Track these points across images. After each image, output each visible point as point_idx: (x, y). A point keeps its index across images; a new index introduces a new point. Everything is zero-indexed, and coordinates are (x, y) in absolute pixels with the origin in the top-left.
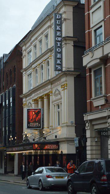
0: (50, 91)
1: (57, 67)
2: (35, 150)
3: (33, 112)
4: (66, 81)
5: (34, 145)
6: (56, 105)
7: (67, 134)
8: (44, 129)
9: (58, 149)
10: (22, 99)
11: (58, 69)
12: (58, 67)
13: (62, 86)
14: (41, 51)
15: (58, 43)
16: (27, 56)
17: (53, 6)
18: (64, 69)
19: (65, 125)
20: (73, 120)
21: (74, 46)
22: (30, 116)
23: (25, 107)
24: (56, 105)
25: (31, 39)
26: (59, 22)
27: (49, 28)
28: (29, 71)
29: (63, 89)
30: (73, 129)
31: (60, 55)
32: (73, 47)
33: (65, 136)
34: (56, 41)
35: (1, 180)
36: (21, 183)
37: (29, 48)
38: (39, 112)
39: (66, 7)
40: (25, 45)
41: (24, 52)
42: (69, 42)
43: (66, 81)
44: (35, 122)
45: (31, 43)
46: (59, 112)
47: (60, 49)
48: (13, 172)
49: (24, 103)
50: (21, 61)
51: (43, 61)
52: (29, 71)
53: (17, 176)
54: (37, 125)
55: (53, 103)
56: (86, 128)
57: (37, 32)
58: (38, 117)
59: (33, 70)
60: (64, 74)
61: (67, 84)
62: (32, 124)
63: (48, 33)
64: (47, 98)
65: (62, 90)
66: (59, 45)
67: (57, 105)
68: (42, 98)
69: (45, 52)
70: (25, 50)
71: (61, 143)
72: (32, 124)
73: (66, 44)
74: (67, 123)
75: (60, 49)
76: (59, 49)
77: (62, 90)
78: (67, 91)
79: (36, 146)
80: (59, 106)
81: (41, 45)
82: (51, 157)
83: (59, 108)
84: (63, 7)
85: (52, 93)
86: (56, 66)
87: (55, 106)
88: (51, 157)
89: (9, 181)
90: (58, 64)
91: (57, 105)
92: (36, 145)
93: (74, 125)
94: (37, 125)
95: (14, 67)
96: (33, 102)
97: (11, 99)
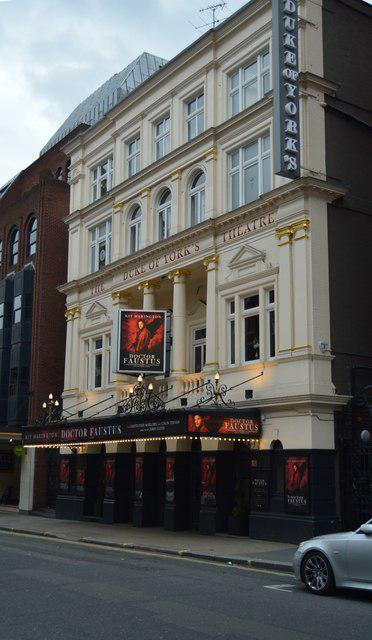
0: (212, 257)
1: (288, 163)
2: (193, 434)
3: (140, 323)
4: (306, 212)
5: (190, 419)
6: (91, 340)
8: (173, 375)
9: (258, 435)
10: (63, 297)
11: (289, 167)
13: (278, 230)
14: (130, 169)
16: (87, 178)
17: (120, 89)
19: (305, 352)
20: (327, 340)
21: (327, 109)
22: (129, 332)
23: (73, 320)
25: (113, 124)
26: (291, 21)
27: (207, 72)
29: (286, 239)
30: (326, 368)
31: (295, 125)
32: (322, 112)
33: (306, 391)
36: (126, 547)
37: (107, 150)
38: (159, 323)
40: (84, 147)
41: (79, 168)
42: (314, 93)
43: (306, 212)
44: (145, 351)
45: (116, 136)
48: (15, 501)
49: (69, 308)
50: (64, 189)
51: (143, 191)
52: (102, 215)
53: (30, 513)
54: (149, 361)
57: (198, 59)
58: (156, 336)
59: (119, 209)
60: (302, 188)
62: (133, 359)
63: (139, 133)
64: (183, 283)
65: (115, 305)
66: (291, 93)
67: (265, 289)
69: (154, 164)
70: (83, 162)
72: (133, 359)
74: (309, 346)
77: (115, 305)
78: (310, 244)
79: (197, 420)
80: (272, 294)
81: (158, 134)
82: (139, 462)
85: (79, 312)
86: (282, 159)
88: (139, 462)
90: (291, 153)
92: (196, 417)
93: (329, 354)
94: (149, 361)
95: (30, 216)
96: (117, 300)
97: (18, 302)
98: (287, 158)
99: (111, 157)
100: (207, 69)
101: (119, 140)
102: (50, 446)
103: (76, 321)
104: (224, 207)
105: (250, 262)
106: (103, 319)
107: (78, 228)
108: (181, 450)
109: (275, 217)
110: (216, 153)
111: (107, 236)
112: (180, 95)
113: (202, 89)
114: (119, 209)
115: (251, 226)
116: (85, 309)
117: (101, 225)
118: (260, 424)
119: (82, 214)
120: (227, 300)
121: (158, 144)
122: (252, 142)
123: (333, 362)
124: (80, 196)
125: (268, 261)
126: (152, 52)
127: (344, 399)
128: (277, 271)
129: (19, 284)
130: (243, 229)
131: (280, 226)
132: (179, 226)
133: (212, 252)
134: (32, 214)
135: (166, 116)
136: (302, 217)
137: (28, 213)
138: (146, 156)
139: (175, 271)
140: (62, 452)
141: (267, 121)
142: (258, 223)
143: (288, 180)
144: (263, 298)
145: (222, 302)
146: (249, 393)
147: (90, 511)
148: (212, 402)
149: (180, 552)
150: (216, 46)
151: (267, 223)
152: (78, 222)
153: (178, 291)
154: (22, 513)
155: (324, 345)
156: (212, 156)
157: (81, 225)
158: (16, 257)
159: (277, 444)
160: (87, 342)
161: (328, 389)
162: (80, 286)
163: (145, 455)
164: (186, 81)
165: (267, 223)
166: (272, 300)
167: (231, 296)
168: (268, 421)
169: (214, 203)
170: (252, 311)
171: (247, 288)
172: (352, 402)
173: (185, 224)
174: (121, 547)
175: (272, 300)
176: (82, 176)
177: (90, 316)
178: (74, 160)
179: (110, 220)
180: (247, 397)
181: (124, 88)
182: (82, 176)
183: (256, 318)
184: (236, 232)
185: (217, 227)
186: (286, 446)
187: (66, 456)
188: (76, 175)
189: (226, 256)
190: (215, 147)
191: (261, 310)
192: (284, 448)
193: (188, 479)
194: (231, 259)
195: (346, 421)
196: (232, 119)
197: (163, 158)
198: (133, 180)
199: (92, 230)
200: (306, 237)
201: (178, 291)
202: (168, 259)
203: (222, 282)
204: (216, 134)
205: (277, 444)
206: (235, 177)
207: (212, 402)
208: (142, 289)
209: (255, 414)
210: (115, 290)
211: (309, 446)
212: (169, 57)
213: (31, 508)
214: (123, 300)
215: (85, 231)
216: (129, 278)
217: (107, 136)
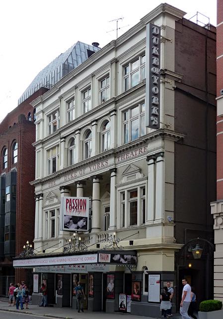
7: (162, 239)
10: (33, 187)
11: (154, 123)
12: (155, 120)
15: (155, 77)
18: (161, 126)
24: (48, 212)
26: (157, 40)
28: (50, 145)
34: (152, 74)
35: (2, 310)
39: (166, 18)
46: (144, 201)
47: (157, 89)
52: (50, 145)
55: (44, 209)
56: (215, 227)
61: (163, 153)
63: (145, 51)
66: (155, 81)
67: (141, 188)
68: (86, 185)
70: (43, 112)
71: (141, 253)
73: (164, 83)
75: (157, 89)
76: (156, 89)
83: (144, 194)
84: (160, 17)
87: (47, 212)
89: (31, 314)
91: (141, 188)
95: (13, 142)
100: (111, 62)
119: (42, 142)
127: (179, 246)
134: (15, 140)
145: (119, 193)
156: (113, 113)
167: (136, 187)
170: (133, 199)
180: (130, 244)
184: (125, 157)
188: (39, 119)
202: (134, 153)
217: (56, 98)
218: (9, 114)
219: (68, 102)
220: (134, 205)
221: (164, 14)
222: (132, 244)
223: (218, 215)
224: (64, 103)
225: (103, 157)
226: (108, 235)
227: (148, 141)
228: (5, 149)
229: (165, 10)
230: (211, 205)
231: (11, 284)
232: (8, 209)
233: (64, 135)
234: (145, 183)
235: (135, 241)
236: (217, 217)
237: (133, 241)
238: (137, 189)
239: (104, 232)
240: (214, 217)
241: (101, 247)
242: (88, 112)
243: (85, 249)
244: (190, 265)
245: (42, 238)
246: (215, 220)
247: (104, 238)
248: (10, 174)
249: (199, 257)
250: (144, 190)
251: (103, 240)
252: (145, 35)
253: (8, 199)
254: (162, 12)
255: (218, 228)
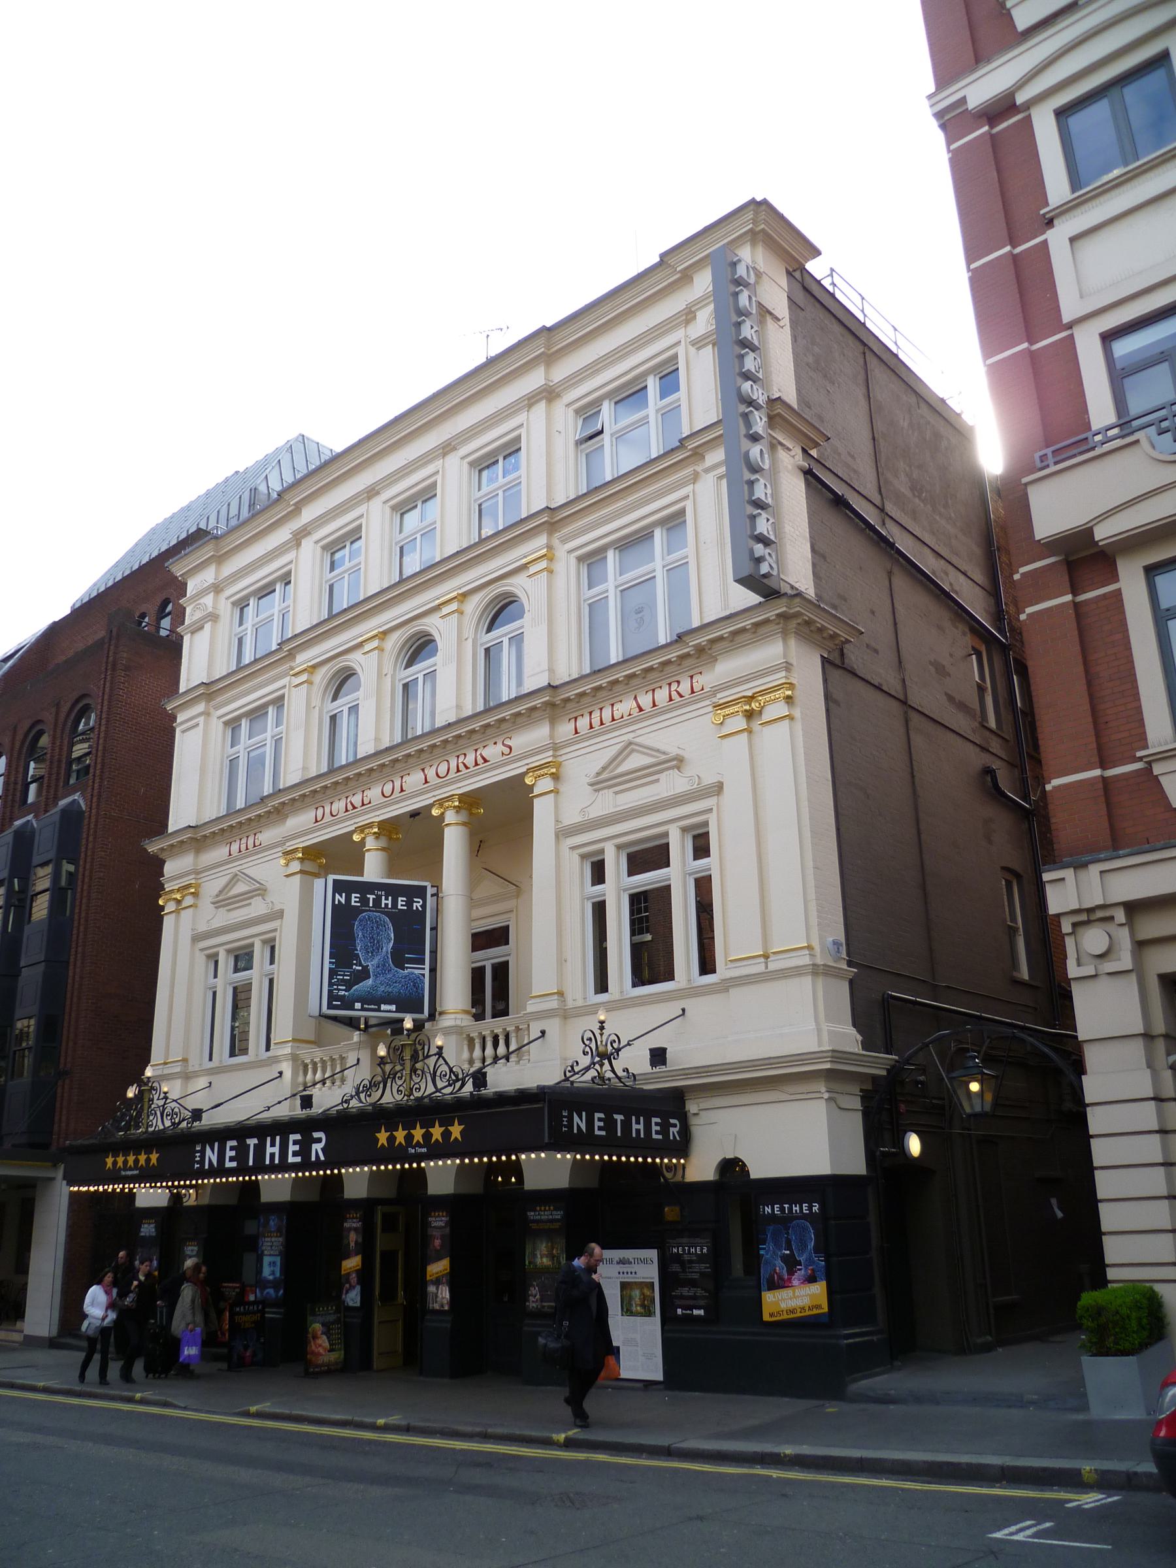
0: (189, 886)
4: (788, 667)
9: (683, 1147)
17: (255, 490)
19: (804, 960)
25: (297, 509)
27: (530, 406)
29: (739, 723)
33: (810, 1045)
41: (208, 600)
50: (173, 649)
64: (464, 824)
67: (264, 942)
70: (217, 588)
74: (809, 948)
87: (598, 874)
91: (264, 942)
95: (77, 701)
98: (759, 549)
99: (286, 580)
100: (530, 401)
101: (308, 544)
102: (118, 1188)
103: (186, 915)
104: (570, 665)
105: (246, 897)
106: (258, 907)
107: (201, 719)
108: (462, 1191)
109: (707, 679)
110: (551, 560)
111: (269, 734)
112: (464, 451)
113: (518, 439)
114: (304, 677)
115: (645, 700)
116: (212, 886)
117: (257, 714)
118: (684, 1118)
119: (210, 691)
120: (209, 957)
121: (331, 587)
122: (642, 537)
123: (851, 982)
124: (200, 660)
125: (689, 770)
126: (313, 434)
127: (879, 1064)
128: (719, 788)
129: (45, 846)
130: (625, 706)
131: (722, 697)
132: (305, 769)
133: (547, 757)
134: (39, 722)
135: (427, 494)
136: (779, 677)
137: (75, 695)
138: (373, 568)
139: (450, 798)
140: (140, 1203)
141: (767, 461)
142: (662, 695)
143: (754, 599)
144: (260, 954)
145: (201, 959)
146: (658, 1056)
147: (258, 1346)
148: (592, 1073)
149: (138, 1395)
150: (549, 359)
151: (357, 803)
152: (200, 707)
153: (454, 842)
154: (32, 1342)
155: (835, 943)
156: (543, 564)
157: (206, 714)
158: (33, 788)
159: (731, 1167)
160: (214, 959)
161: (850, 1039)
162: (200, 838)
163: (366, 1206)
164: (472, 428)
165: (357, 803)
166: (272, 962)
167: (215, 950)
168: (705, 1117)
169: (546, 651)
170: (648, 879)
171: (639, 828)
172: (894, 1072)
173: (390, 736)
174: (373, 1427)
175: (272, 962)
176: (213, 617)
177: (223, 901)
178: (192, 587)
179: (279, 702)
180: (654, 1063)
181: (262, 488)
182: (213, 617)
183: (248, 987)
184: (607, 714)
185: (555, 702)
186: (763, 1166)
187: (150, 1213)
188: (198, 615)
189: (583, 764)
190: (549, 557)
191: (255, 976)
192: (753, 1176)
193: (463, 1249)
194: (598, 768)
195: (883, 1108)
196: (505, 530)
197: (488, 538)
198: (335, 621)
199: (233, 725)
200: (790, 717)
201: (454, 842)
202: (431, 773)
203: (571, 817)
204: (552, 520)
205: (731, 1167)
206: (233, 762)
207: (592, 1073)
208: (363, 842)
209: (672, 1104)
210: (290, 846)
211: (822, 1167)
212: (339, 448)
213: (54, 1333)
214: (309, 866)
215: (216, 726)
216: (328, 818)
217: (282, 535)
218: (55, 623)
219: (333, 547)
220: (240, 998)
221: (753, 236)
222: (664, 1063)
223: (1084, 917)
224: (309, 551)
225: (496, 719)
226: (342, 1059)
227: (286, 808)
228: (40, 733)
229: (763, 224)
230: (1046, 877)
231: (137, 1263)
232: (33, 952)
233: (320, 655)
234: (275, 930)
235: (316, 1092)
236: (1075, 925)
237: (664, 1050)
238: (252, 945)
239: (492, 1025)
240: (1066, 927)
241: (317, 1109)
242: (256, 661)
243: (184, 1125)
244: (914, 1145)
245: (185, 1060)
246: (1070, 943)
247: (318, 1076)
248: (57, 818)
249: (989, 1097)
250: (273, 948)
251: (323, 1082)
252: (703, 282)
253: (41, 908)
254: (751, 230)
255: (1089, 970)
